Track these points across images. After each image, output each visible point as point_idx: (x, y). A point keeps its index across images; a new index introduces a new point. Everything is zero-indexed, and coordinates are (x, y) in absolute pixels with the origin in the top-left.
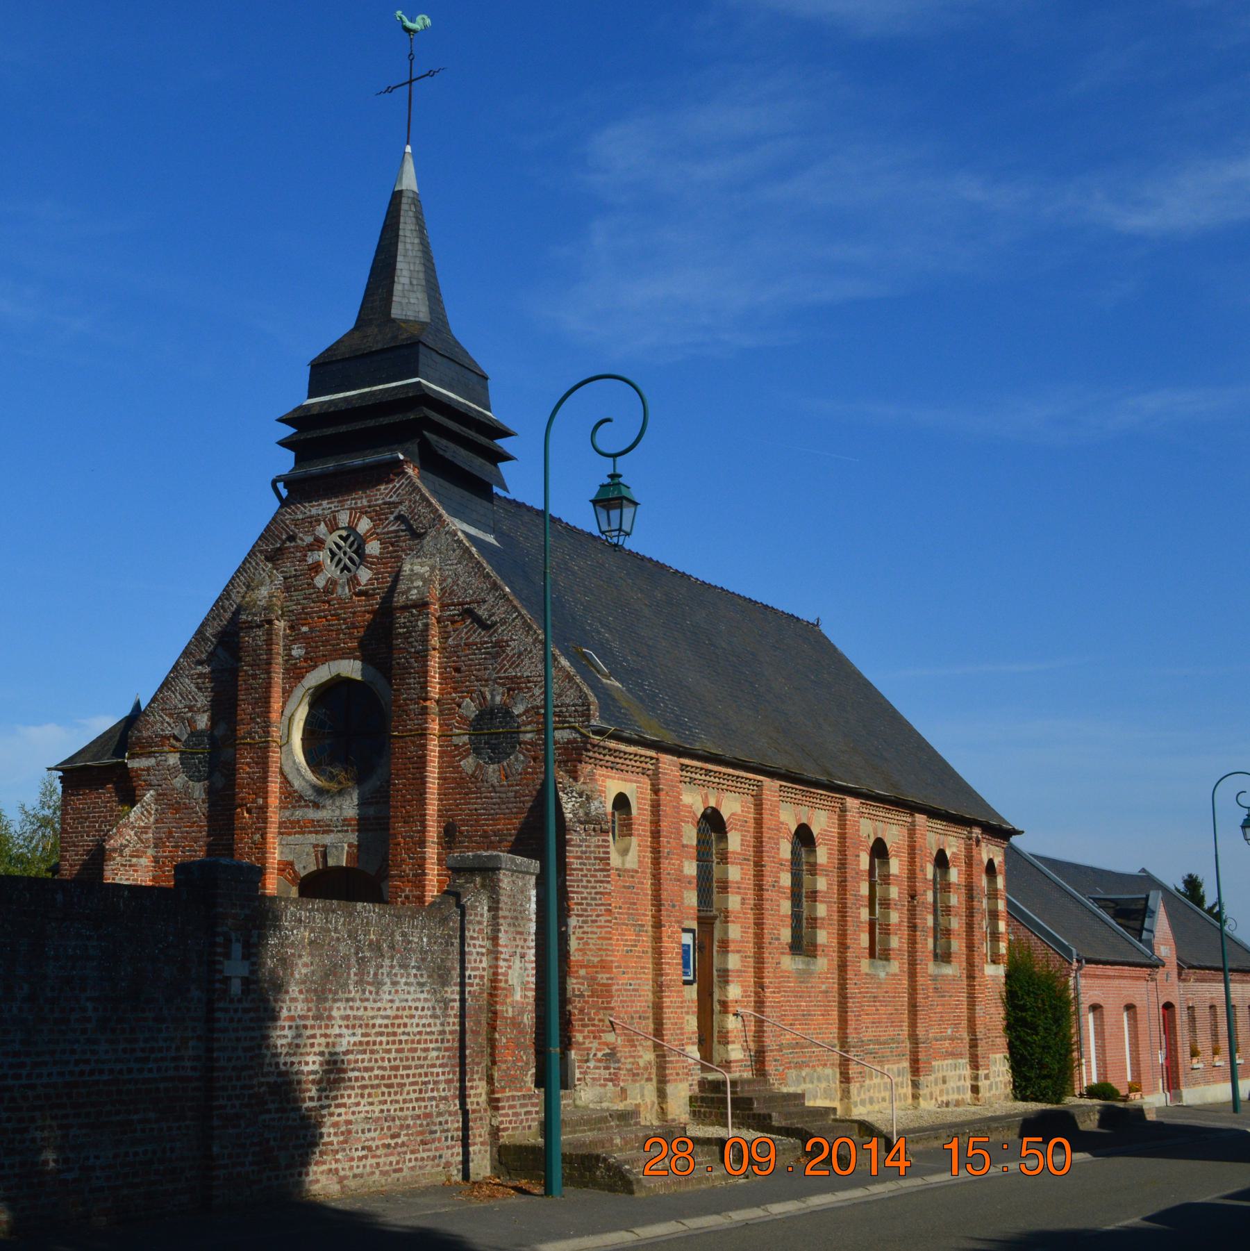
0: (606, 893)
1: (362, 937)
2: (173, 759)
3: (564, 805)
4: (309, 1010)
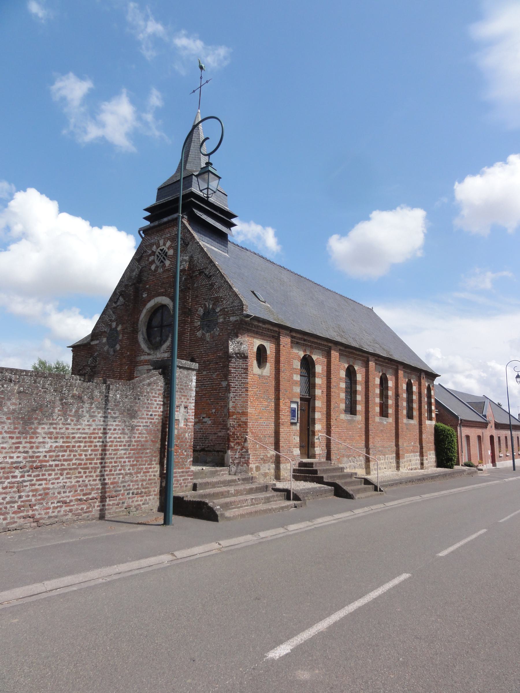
0: (246, 383)
1: (67, 392)
2: (104, 340)
3: (230, 346)
4: (15, 428)
